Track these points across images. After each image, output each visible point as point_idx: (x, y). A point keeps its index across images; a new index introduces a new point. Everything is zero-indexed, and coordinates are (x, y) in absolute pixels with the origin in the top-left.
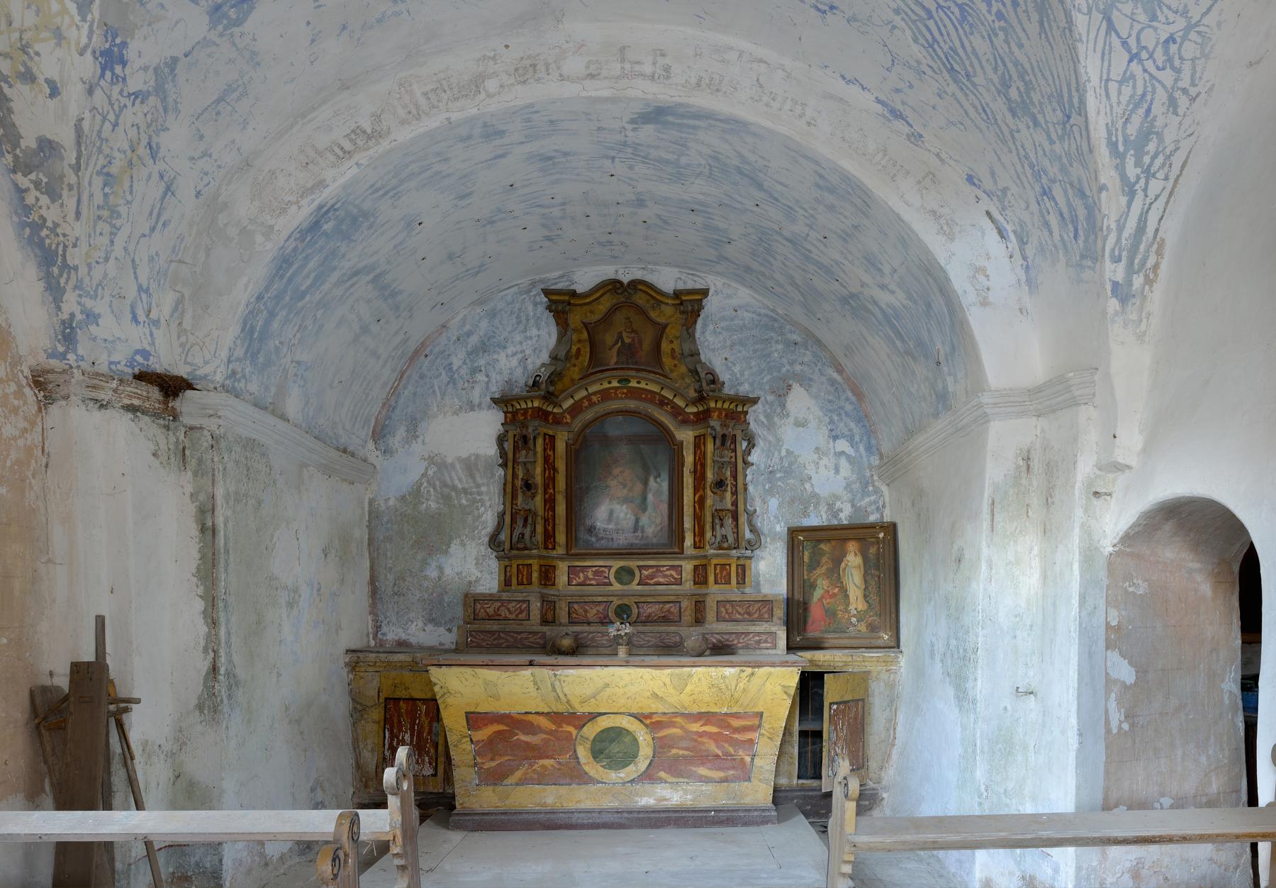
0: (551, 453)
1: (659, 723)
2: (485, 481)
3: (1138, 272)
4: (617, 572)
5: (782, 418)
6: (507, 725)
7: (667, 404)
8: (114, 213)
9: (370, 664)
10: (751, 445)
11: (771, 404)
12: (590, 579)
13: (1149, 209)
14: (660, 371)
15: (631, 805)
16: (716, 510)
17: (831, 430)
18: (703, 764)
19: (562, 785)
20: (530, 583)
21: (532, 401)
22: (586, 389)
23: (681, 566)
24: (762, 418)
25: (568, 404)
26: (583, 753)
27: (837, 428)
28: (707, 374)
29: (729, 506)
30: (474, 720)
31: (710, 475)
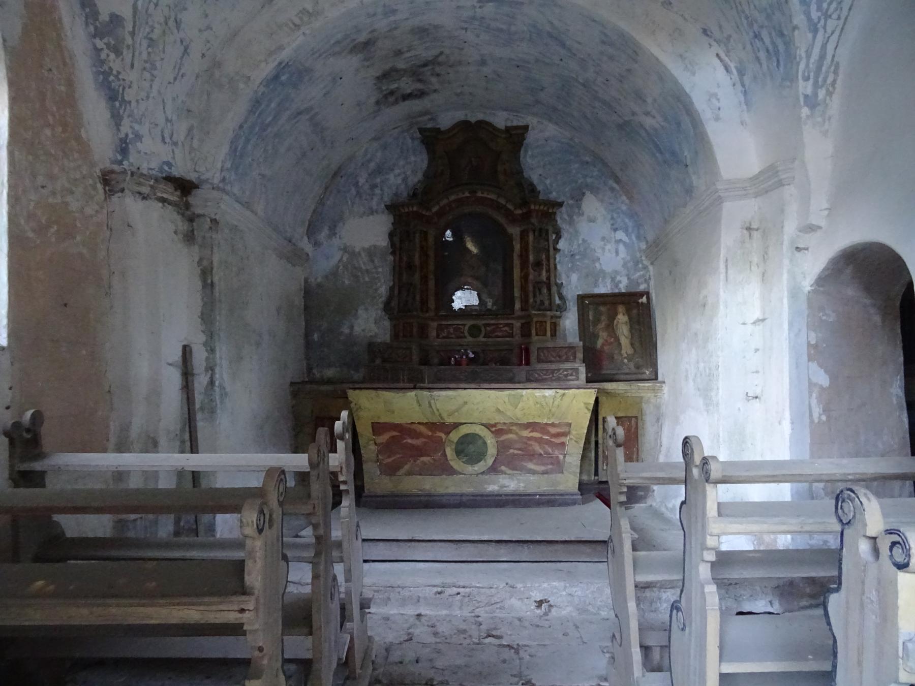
3: (821, 87)
8: (154, 67)
10: (559, 237)
12: (452, 334)
13: (828, 41)
18: (531, 460)
24: (566, 217)
25: (435, 209)
26: (450, 452)
30: (378, 428)
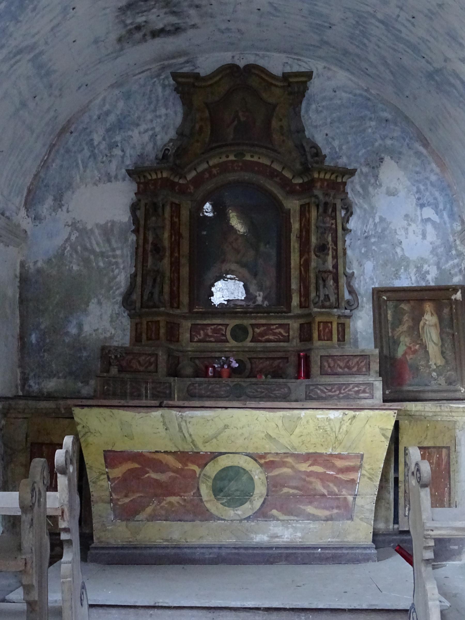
0: (176, 220)
1: (272, 462)
2: (120, 245)
4: (233, 330)
5: (375, 188)
6: (139, 463)
7: (277, 176)
9: (20, 410)
10: (349, 213)
11: (366, 175)
14: (270, 146)
15: (245, 541)
16: (319, 271)
17: (419, 199)
18: (310, 503)
19: (187, 521)
20: (158, 338)
21: (161, 172)
22: (208, 162)
23: (289, 324)
24: (358, 188)
27: (424, 196)
28: (311, 148)
29: (331, 268)
31: (314, 240)
